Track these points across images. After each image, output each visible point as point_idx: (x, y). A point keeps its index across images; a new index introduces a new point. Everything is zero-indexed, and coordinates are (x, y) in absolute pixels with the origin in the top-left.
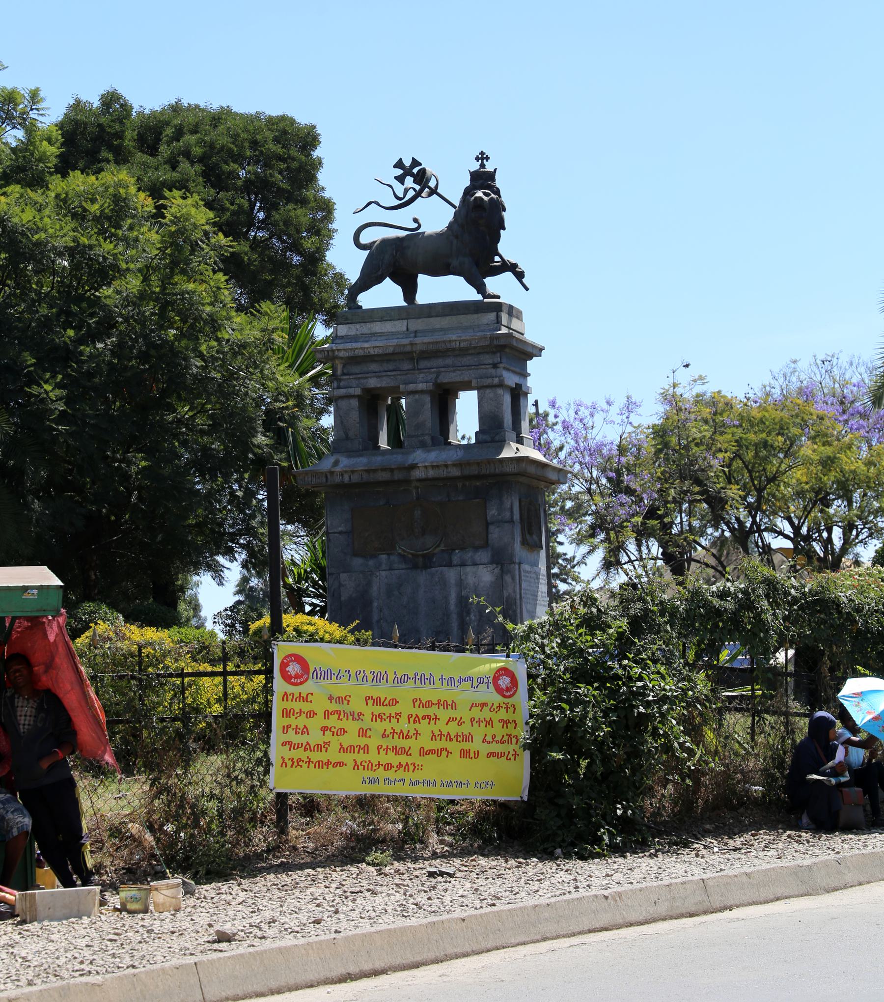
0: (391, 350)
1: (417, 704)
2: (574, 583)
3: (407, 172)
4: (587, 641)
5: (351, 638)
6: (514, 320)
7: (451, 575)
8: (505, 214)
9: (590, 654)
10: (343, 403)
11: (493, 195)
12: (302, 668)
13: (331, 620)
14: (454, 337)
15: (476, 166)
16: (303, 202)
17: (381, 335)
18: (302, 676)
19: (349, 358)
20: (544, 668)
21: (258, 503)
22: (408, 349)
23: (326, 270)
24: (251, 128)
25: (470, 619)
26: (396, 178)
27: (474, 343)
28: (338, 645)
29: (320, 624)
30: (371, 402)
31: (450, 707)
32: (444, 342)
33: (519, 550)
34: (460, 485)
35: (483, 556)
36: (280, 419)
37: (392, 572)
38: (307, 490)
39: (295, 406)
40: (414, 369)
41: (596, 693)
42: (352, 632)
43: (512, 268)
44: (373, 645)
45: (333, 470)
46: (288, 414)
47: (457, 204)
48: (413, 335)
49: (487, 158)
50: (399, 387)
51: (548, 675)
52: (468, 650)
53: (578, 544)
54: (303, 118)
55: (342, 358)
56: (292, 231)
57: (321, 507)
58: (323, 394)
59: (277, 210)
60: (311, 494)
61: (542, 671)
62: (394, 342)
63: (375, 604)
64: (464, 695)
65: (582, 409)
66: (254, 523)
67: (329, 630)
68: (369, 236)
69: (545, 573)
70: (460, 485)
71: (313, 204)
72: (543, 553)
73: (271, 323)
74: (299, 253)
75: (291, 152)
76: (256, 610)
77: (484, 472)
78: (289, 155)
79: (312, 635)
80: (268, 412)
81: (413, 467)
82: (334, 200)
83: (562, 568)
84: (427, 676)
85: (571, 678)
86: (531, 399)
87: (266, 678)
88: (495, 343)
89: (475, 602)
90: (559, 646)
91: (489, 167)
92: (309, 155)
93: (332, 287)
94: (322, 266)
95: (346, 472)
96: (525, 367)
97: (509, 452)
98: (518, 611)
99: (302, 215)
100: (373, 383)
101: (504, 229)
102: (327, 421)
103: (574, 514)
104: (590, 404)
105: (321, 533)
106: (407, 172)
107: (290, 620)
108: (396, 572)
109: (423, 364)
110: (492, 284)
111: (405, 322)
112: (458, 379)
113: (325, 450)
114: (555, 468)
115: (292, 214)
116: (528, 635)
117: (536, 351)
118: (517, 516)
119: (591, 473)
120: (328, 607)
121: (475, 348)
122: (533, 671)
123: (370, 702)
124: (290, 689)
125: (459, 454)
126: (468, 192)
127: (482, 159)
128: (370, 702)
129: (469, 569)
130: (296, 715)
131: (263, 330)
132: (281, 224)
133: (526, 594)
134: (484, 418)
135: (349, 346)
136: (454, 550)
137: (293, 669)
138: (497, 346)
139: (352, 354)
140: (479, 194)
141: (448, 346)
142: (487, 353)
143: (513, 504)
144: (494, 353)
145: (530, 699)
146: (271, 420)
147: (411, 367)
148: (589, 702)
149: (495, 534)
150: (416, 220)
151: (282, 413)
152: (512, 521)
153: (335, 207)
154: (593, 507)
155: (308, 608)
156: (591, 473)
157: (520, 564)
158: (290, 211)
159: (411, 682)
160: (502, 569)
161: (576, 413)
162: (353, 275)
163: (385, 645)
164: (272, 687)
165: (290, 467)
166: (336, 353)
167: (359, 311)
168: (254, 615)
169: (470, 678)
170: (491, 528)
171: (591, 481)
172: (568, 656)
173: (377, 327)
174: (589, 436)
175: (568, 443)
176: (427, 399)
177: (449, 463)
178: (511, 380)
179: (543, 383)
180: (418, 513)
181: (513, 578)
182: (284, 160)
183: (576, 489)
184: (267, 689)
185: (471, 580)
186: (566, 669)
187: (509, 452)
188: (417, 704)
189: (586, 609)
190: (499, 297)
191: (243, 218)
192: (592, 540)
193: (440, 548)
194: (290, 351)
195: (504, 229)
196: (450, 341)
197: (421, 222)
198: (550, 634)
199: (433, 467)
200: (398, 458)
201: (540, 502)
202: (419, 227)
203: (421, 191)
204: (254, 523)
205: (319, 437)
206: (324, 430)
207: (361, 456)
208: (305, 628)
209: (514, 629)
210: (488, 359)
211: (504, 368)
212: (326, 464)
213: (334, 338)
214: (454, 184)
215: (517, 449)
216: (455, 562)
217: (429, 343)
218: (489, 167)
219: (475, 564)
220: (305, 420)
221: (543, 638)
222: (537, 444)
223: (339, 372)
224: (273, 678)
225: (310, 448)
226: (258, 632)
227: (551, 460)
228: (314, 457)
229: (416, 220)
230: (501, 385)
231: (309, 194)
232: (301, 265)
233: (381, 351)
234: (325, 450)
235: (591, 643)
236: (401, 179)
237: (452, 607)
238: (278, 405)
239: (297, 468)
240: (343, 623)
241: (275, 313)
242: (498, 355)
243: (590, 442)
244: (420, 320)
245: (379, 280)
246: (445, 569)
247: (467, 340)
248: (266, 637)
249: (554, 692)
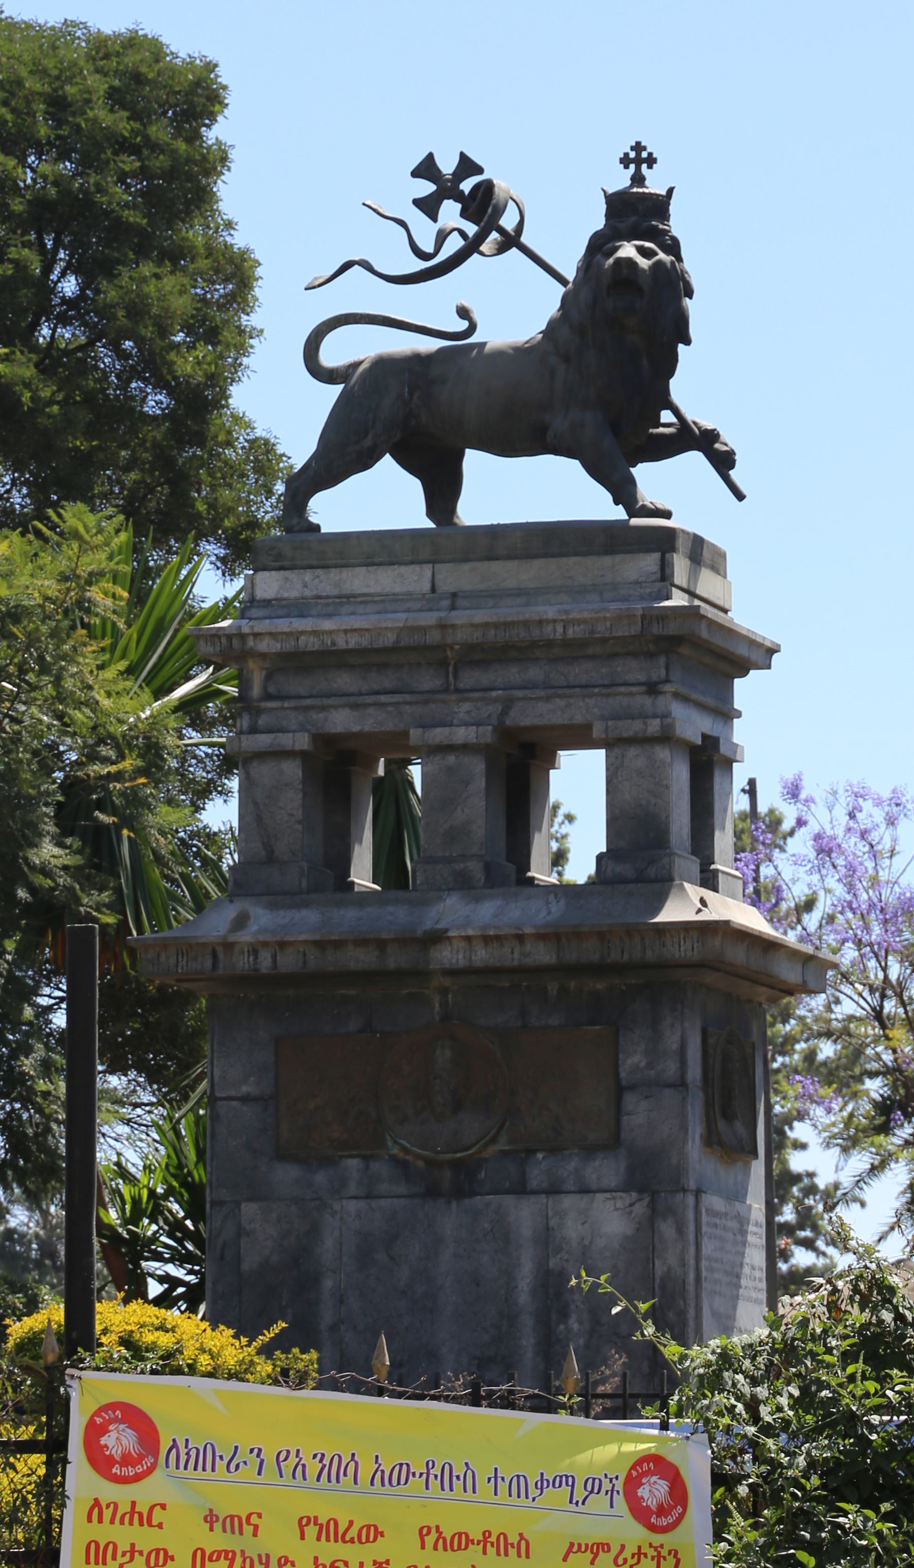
0: (389, 639)
1: (430, 1540)
2: (831, 1251)
3: (447, 189)
4: (867, 1395)
5: (265, 1367)
6: (706, 575)
7: (524, 1215)
8: (691, 305)
9: (872, 1428)
10: (264, 771)
11: (662, 256)
12: (141, 1441)
13: (214, 1320)
14: (550, 612)
15: (621, 180)
16: (175, 256)
17: (365, 599)
18: (141, 1458)
19: (284, 656)
20: (755, 1459)
21: (37, 1016)
22: (434, 637)
23: (229, 432)
24: (49, 63)
25: (569, 1330)
26: (418, 203)
27: (602, 630)
28: (233, 1384)
29: (189, 1328)
30: (335, 770)
31: (512, 1552)
32: (526, 624)
33: (697, 1159)
34: (553, 987)
35: (606, 1170)
36: (101, 805)
37: (374, 1203)
38: (161, 989)
39: (139, 772)
40: (446, 691)
41: (886, 1527)
42: (267, 1351)
43: (705, 441)
44: (320, 1386)
45: (231, 939)
46: (122, 794)
47: (570, 274)
48: (446, 603)
49: (651, 161)
50: (406, 734)
51: (765, 1478)
52: (563, 1406)
53: (845, 1150)
54: (183, 42)
55: (263, 656)
56: (148, 331)
57: (198, 1033)
58: (211, 745)
59: (111, 276)
60: (171, 1000)
61: (749, 1468)
62: (397, 620)
63: (328, 1284)
64: (549, 1522)
65: (867, 805)
66: (28, 1064)
67: (209, 1344)
68: (344, 349)
69: (762, 1219)
70: (553, 987)
71: (203, 264)
72: (758, 1168)
73: (85, 559)
74: (160, 384)
75: (152, 130)
76: (23, 1289)
77: (615, 956)
78: (146, 138)
79: (169, 1355)
80: (67, 786)
81: (436, 938)
82: (258, 255)
83: (806, 1218)
84: (459, 1470)
85: (823, 1487)
86: (740, 775)
87: (48, 1463)
88: (656, 630)
89: (585, 1287)
90: (796, 1404)
92: (199, 136)
93: (243, 475)
94: (219, 421)
95: (265, 944)
96: (727, 694)
97: (678, 910)
98: (692, 1312)
99: (171, 291)
100: (341, 721)
101: (688, 342)
102: (221, 814)
103: (842, 1077)
104: (886, 794)
105: (194, 1097)
106: (447, 189)
107: (112, 1315)
108: (383, 1202)
109: (470, 678)
110: (653, 479)
111: (427, 570)
112: (558, 719)
113: (214, 891)
114: (794, 954)
115: (151, 288)
116: (718, 1375)
117: (756, 655)
118: (694, 1073)
119: (885, 969)
120: (208, 1286)
121: (604, 641)
122: (729, 1466)
123: (311, 1531)
124: (109, 1491)
125: (554, 908)
126: (599, 245)
127: (638, 161)
128: (311, 1531)
129: (568, 1202)
130: (120, 1560)
131: (64, 578)
132: (121, 313)
133: (711, 1270)
134: (618, 819)
135: (283, 625)
136: (531, 1152)
137: (119, 1440)
138: (659, 639)
139: (289, 646)
140: (628, 250)
141: (536, 633)
142: (634, 655)
143: (685, 1040)
144: (651, 656)
145: (718, 1537)
146: (78, 810)
147: (438, 683)
148: (867, 1550)
149: (638, 1114)
150: (463, 313)
151: (105, 788)
152: (681, 1084)
153: (259, 271)
154: (888, 1057)
155: (155, 1289)
156: (885, 969)
157: (698, 1193)
158: (144, 280)
159: (417, 1483)
160: (652, 1206)
161: (852, 815)
162: (298, 446)
163: (356, 1388)
164: (62, 1484)
165: (123, 926)
166: (251, 642)
167: (311, 537)
168: (18, 1300)
169: (568, 1480)
170: (630, 1100)
171: (884, 989)
172: (817, 1430)
173: (358, 580)
174: (883, 875)
175: (828, 891)
176: (478, 766)
177: (528, 930)
178: (692, 725)
179: (770, 734)
180: (444, 1055)
181: (680, 1230)
182: (135, 150)
183: (847, 1007)
184: (51, 1491)
185: (572, 1230)
186: (812, 1464)
187: (678, 910)
188: (430, 1540)
189: (866, 1315)
190: (667, 515)
191: (25, 295)
192: (881, 1139)
193: (497, 1147)
194: (134, 631)
195: (688, 342)
196: (540, 622)
197: (476, 316)
198: (771, 1373)
199: (487, 940)
200: (397, 916)
201: (755, 1036)
202: (472, 329)
203: (480, 238)
204: (28, 1064)
205: (197, 855)
206: (210, 838)
207: (306, 905)
208: (149, 1337)
209: (683, 1358)
210: (634, 670)
211: (677, 695)
212: (216, 925)
213: (248, 604)
214: (564, 223)
215: (703, 902)
216: (533, 1184)
217: (487, 625)
218: (655, 184)
219: (585, 1190)
220: (164, 809)
221: (755, 1382)
222: (750, 889)
223: (256, 690)
224: (65, 1461)
225: (173, 881)
226: (31, 1344)
227: (785, 933)
228: (183, 905)
229: (463, 313)
230: (666, 738)
231: (195, 234)
232: (170, 416)
233: (365, 642)
234: (214, 891)
235: (877, 1401)
236: (429, 206)
237: (524, 1297)
238: (97, 769)
239: (140, 931)
240: (246, 1329)
241: (96, 533)
242: (656, 658)
243: (886, 893)
244: (466, 567)
245: (365, 462)
246: (509, 1200)
247: (584, 621)
248: (51, 1358)
249: (779, 1521)
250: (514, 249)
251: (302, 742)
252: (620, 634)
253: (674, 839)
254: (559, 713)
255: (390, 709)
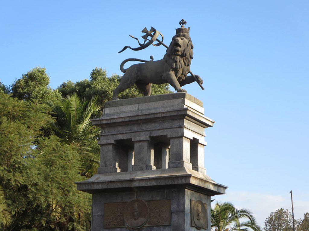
15: (179, 26)
47: (168, 46)
49: (185, 23)
91: (186, 26)
170: (173, 215)
250: (196, 82)
251: (113, 142)
252: (172, 115)
253: (184, 159)
254: (161, 133)
255: (129, 134)
